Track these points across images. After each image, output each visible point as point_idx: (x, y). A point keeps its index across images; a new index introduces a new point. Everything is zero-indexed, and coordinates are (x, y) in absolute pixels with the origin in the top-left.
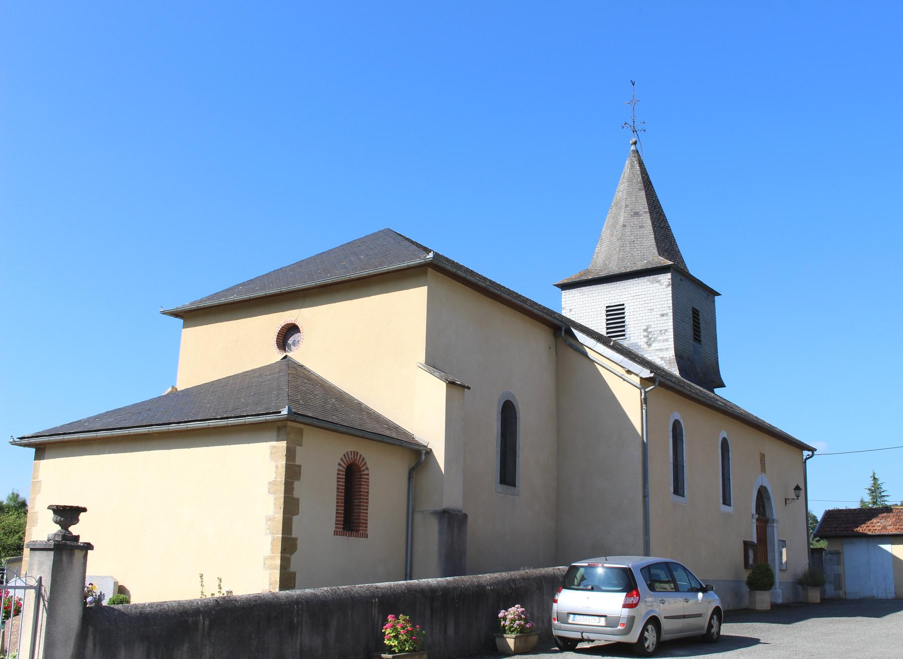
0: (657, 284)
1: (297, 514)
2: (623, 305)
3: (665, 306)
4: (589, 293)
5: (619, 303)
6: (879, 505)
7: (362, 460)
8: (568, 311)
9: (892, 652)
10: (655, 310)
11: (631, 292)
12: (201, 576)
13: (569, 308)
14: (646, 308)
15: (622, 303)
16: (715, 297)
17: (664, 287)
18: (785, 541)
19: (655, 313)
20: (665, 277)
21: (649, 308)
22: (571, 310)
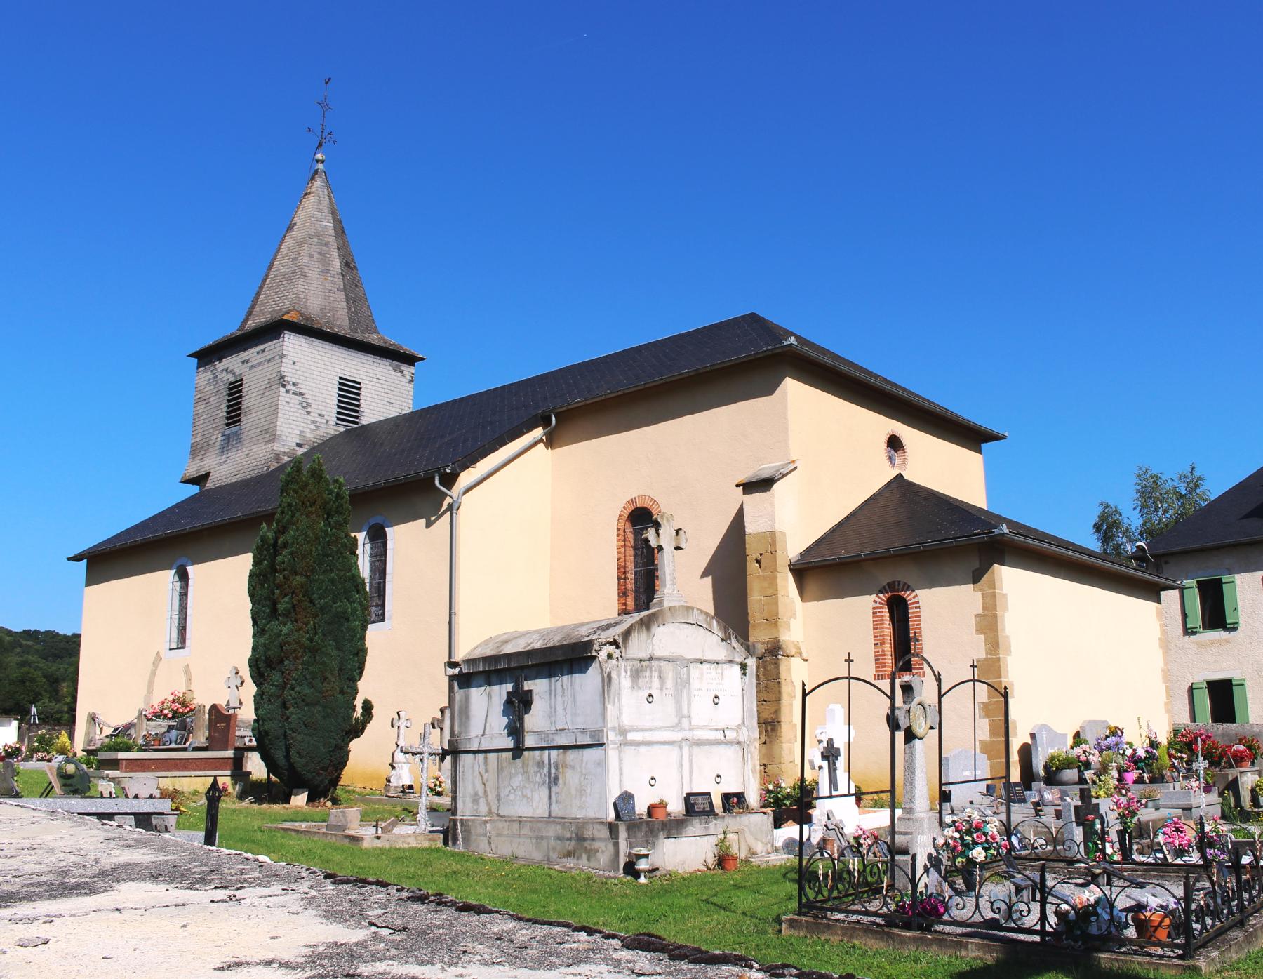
0: (399, 374)
1: (382, 618)
2: (359, 383)
3: (405, 404)
4: (320, 349)
5: (354, 379)
6: (894, 853)
7: (914, 597)
8: (291, 362)
9: (803, 948)
10: (394, 405)
11: (371, 371)
12: (212, 901)
13: (292, 359)
14: (386, 399)
15: (358, 380)
16: (982, 445)
17: (407, 381)
18: (709, 794)
19: (394, 409)
20: (409, 370)
21: (389, 400)
22: (294, 363)
